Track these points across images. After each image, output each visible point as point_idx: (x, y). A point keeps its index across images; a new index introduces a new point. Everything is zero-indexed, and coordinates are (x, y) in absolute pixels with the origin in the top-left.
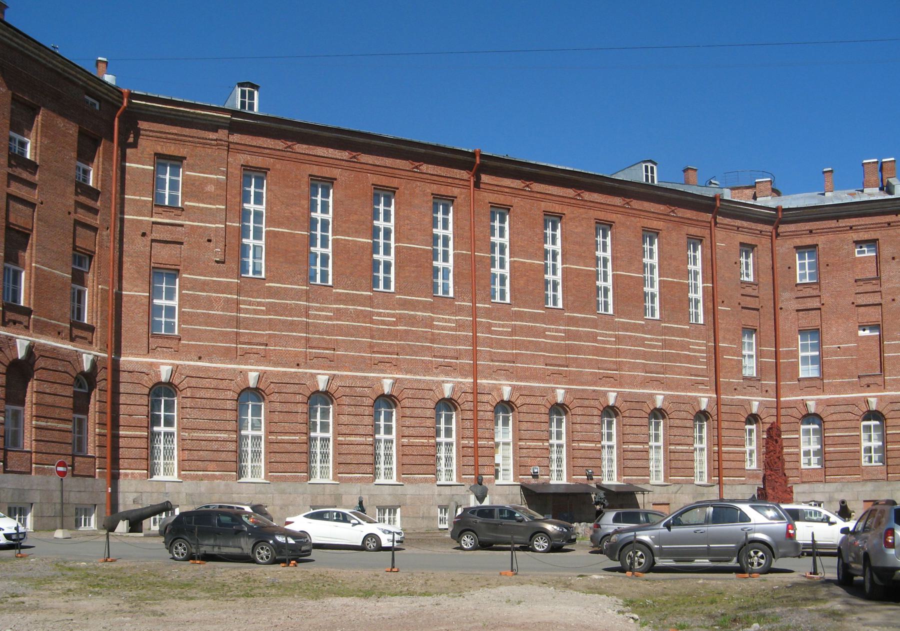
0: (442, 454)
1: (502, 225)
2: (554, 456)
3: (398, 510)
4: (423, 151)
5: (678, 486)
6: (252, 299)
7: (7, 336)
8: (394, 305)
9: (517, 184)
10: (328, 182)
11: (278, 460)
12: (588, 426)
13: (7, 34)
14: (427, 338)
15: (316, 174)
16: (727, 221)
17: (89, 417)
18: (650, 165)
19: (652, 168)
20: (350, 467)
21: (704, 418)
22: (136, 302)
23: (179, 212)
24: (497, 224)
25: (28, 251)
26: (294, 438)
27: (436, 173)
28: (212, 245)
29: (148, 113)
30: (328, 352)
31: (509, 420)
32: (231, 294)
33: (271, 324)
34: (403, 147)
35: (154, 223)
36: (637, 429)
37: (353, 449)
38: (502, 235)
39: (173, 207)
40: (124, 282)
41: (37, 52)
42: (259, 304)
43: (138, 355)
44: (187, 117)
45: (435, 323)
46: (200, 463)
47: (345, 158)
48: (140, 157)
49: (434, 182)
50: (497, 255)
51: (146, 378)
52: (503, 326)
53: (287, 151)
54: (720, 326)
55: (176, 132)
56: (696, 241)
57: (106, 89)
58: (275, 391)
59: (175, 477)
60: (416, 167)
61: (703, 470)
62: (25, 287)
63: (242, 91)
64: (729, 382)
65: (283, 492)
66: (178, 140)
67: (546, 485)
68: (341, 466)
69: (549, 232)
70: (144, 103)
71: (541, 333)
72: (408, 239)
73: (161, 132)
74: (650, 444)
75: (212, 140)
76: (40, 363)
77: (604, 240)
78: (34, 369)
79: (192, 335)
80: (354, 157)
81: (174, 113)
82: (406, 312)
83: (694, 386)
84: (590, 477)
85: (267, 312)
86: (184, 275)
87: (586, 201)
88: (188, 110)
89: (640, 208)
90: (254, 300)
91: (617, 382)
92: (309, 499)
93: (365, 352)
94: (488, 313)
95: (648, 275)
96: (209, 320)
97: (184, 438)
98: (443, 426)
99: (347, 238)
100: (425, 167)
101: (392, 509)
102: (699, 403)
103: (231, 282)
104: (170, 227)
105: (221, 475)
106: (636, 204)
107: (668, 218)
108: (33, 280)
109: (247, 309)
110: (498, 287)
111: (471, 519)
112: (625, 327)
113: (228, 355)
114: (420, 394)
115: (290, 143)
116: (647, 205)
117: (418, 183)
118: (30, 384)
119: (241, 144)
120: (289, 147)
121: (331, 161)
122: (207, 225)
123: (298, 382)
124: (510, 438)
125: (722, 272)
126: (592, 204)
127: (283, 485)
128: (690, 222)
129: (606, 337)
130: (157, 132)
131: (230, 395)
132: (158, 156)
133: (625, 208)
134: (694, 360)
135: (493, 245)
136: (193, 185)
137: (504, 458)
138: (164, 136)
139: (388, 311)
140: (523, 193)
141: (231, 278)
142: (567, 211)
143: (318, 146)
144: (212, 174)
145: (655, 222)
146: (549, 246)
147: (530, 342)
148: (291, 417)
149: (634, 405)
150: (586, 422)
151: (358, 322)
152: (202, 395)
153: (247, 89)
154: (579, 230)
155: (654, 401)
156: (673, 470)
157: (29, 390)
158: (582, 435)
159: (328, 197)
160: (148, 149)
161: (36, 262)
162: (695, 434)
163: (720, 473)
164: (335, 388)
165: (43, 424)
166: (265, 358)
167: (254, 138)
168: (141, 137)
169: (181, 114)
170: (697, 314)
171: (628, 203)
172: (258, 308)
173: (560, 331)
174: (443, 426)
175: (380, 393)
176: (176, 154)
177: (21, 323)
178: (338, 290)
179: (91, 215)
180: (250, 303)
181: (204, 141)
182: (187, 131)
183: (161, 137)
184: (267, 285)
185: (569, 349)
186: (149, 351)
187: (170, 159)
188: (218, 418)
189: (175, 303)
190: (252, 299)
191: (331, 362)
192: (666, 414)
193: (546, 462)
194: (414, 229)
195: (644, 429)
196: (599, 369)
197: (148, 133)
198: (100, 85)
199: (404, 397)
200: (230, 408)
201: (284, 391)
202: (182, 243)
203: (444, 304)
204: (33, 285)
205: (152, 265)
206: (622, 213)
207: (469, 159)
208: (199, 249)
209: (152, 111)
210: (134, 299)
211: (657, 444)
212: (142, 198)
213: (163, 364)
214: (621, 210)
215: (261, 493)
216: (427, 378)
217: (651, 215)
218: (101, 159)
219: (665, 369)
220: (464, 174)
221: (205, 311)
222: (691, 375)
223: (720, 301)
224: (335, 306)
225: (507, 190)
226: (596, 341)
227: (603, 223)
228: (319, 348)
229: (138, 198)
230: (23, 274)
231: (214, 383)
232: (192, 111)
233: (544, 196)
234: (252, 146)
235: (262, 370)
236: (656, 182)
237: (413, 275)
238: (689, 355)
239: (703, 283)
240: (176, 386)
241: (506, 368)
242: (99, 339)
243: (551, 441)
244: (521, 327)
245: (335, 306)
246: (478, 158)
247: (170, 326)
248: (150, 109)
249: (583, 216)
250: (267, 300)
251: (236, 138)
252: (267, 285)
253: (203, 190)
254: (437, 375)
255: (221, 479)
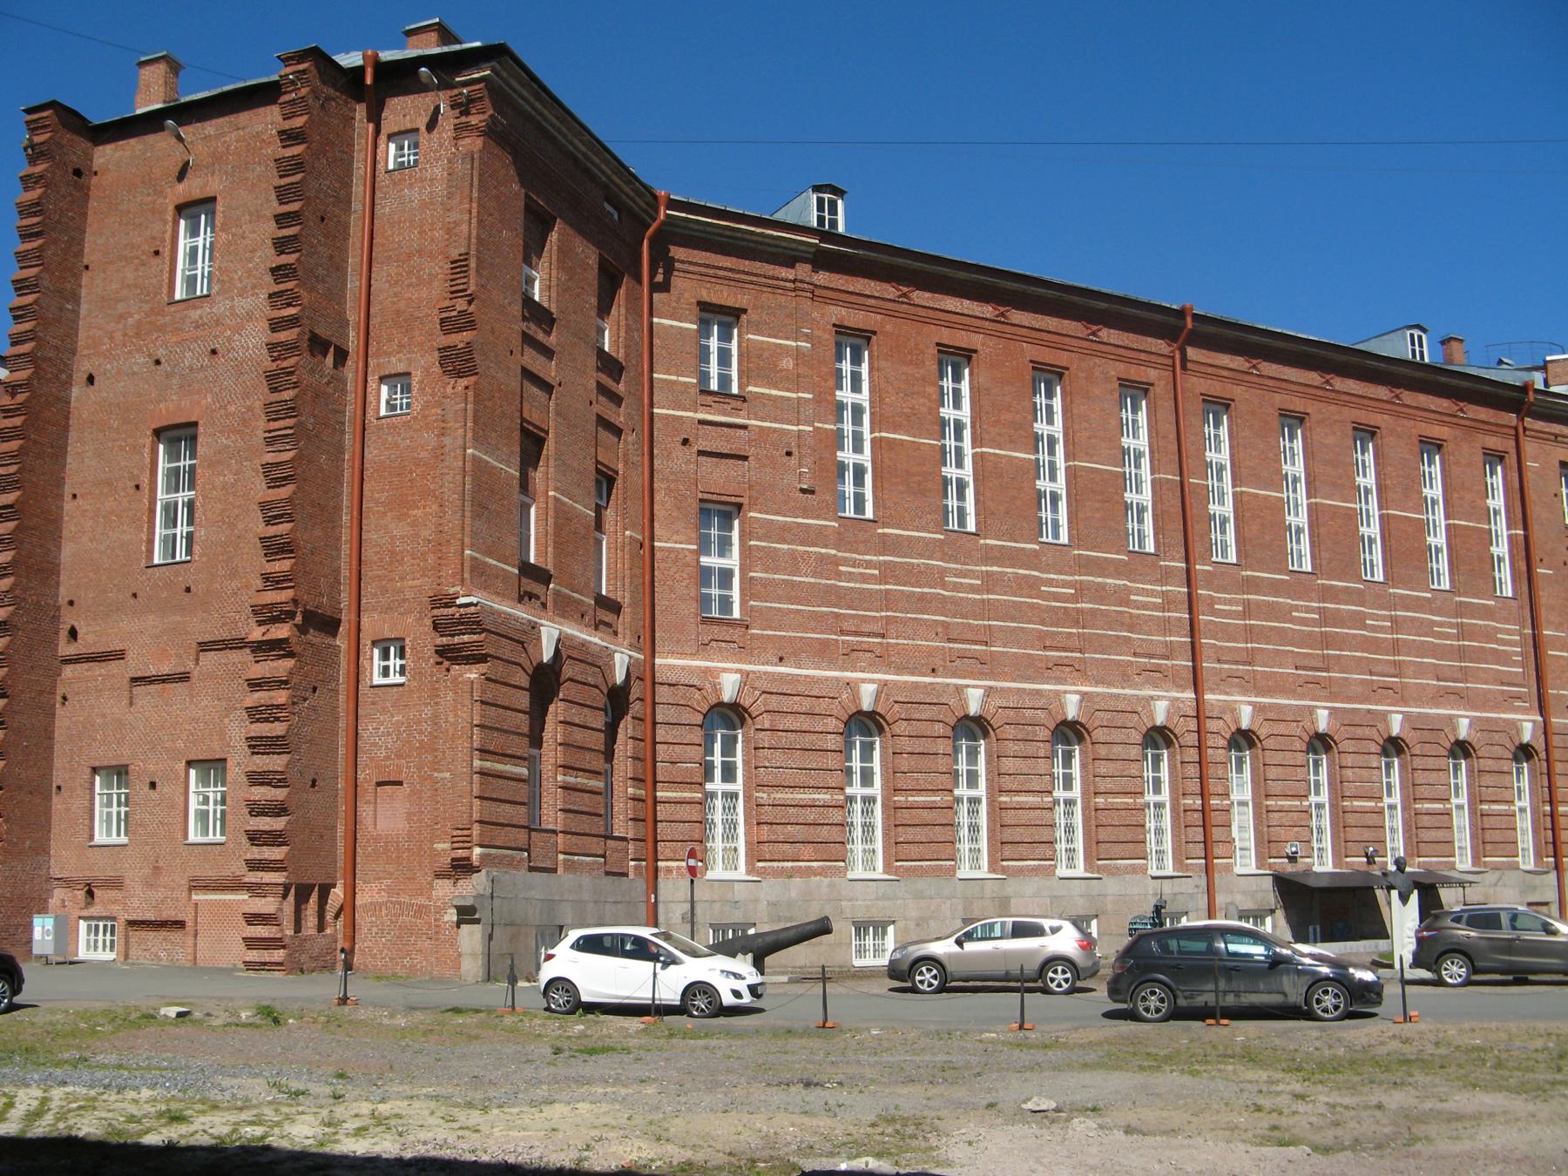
0: (963, 817)
1: (856, 369)
2: (857, 819)
3: (891, 929)
4: (1104, 305)
5: (1497, 874)
6: (858, 557)
7: (529, 621)
8: (1070, 567)
9: (1238, 362)
10: (966, 355)
11: (910, 838)
12: (1364, 772)
13: (525, 94)
14: (1123, 624)
15: (946, 342)
16: (1539, 425)
17: (615, 767)
18: (1416, 333)
19: (1420, 338)
20: (1021, 848)
21: (978, 732)
22: (676, 561)
23: (739, 404)
24: (846, 366)
25: (540, 469)
26: (934, 799)
27: (1121, 343)
28: (793, 461)
29: (687, 232)
30: (977, 647)
31: (872, 749)
32: (826, 547)
33: (888, 600)
34: (1076, 299)
35: (701, 422)
36: (1432, 778)
37: (1025, 817)
38: (856, 388)
39: (724, 394)
40: (656, 525)
41: (558, 124)
42: (869, 565)
43: (682, 655)
44: (748, 241)
45: (1132, 597)
46: (788, 846)
47: (988, 316)
48: (674, 308)
49: (1120, 359)
50: (848, 427)
51: (697, 695)
52: (1230, 602)
53: (903, 303)
54: (1543, 601)
55: (730, 266)
56: (1363, 434)
57: (636, 191)
58: (903, 716)
59: (741, 873)
60: (1094, 334)
61: (1323, 845)
62: (537, 533)
63: (818, 198)
64: (1558, 695)
65: (919, 896)
66: (732, 279)
67: (1308, 872)
68: (1007, 847)
69: (948, 384)
70: (683, 215)
71: (1284, 614)
72: (1087, 454)
73: (708, 266)
74: (957, 792)
75: (786, 280)
76: (568, 670)
77: (957, 386)
78: (562, 680)
79: (770, 619)
80: (1002, 314)
81: (729, 233)
82: (1091, 578)
83: (1508, 701)
84: (1370, 861)
85: (882, 579)
86: (752, 514)
87: (1338, 392)
88: (753, 229)
89: (1414, 404)
90: (861, 557)
91: (1400, 695)
92: (960, 907)
93: (1033, 648)
94: (1210, 579)
95: (1044, 457)
96: (793, 592)
97: (762, 802)
98: (718, 759)
99: (997, 451)
100: (1106, 334)
101: (880, 927)
102: (1519, 731)
103: (826, 526)
104: (725, 429)
105: (822, 867)
106: (1408, 397)
107: (1455, 420)
108: (551, 521)
109: (850, 573)
110: (849, 488)
111: (1455, 932)
112: (1406, 603)
113: (823, 653)
114: (1120, 720)
115: (905, 289)
116: (1424, 400)
117: (1097, 360)
118: (552, 708)
119: (832, 289)
120: (904, 295)
121: (968, 321)
122: (785, 426)
123: (935, 701)
124: (1247, 795)
125: (1537, 511)
126: (1347, 398)
127: (921, 884)
128: (1486, 427)
129: (964, 580)
130: (700, 265)
131: (832, 724)
132: (704, 306)
133: (1394, 403)
134: (1502, 658)
135: (840, 407)
136: (760, 356)
137: (1243, 828)
138: (712, 272)
139: (1062, 577)
140: (1247, 378)
141: (826, 519)
142: (1312, 408)
143: (947, 294)
144: (787, 339)
145: (1437, 428)
146: (947, 412)
147: (1272, 628)
148: (926, 762)
149: (1428, 736)
150: (1360, 764)
151: (1021, 596)
152: (788, 726)
153: (826, 196)
154: (1330, 440)
155: (1455, 729)
156: (1489, 847)
157: (549, 718)
158: (1356, 787)
159: (729, 340)
160: (686, 295)
161: (556, 489)
162: (1145, 774)
163: (1209, 851)
164: (992, 711)
165: (571, 780)
166: (882, 659)
167: (850, 278)
168: (676, 273)
169: (739, 235)
170: (962, 513)
171: (1397, 397)
172: (867, 571)
173: (1311, 610)
174: (718, 759)
175: (1059, 719)
176: (729, 304)
177: (538, 598)
178: (988, 541)
179: (613, 406)
180: (855, 564)
181: (775, 282)
182: (746, 265)
183: (709, 275)
184: (880, 531)
185: (1326, 641)
186: (703, 648)
187: (719, 313)
188: (814, 766)
189: (733, 561)
190: (858, 557)
191: (985, 666)
192: (884, 724)
193: (1304, 833)
194: (1096, 437)
195: (1042, 766)
196: (1371, 673)
197: (685, 267)
198: (628, 183)
199: (1096, 725)
200: (833, 748)
201: (916, 716)
202: (745, 458)
203: (1139, 564)
204: (551, 530)
205: (700, 495)
206: (1391, 413)
207: (1172, 320)
208: (774, 468)
209: (693, 230)
210: (673, 556)
211: (868, 791)
212: (681, 379)
213: (725, 670)
214: (1389, 407)
215: (885, 897)
216: (1128, 691)
217: (1432, 416)
218: (623, 310)
219: (1465, 675)
220: (1160, 346)
221: (786, 577)
222: (1502, 684)
223: (1538, 558)
224: (984, 568)
225: (1225, 373)
226: (1365, 627)
227: (952, 353)
228: (963, 641)
229: (674, 378)
230: (533, 510)
231: (806, 704)
232: (759, 230)
233: (1277, 384)
234: (848, 292)
235: (880, 680)
236: (1427, 360)
237: (1098, 515)
238: (1497, 650)
239: (1509, 528)
240: (746, 710)
241: (1240, 674)
242: (627, 625)
243: (848, 791)
244: (1258, 604)
245: (984, 568)
246: (1189, 320)
247: (726, 603)
248: (691, 225)
249: (1336, 417)
250: (881, 558)
251: (822, 278)
252: (880, 531)
253: (776, 366)
254: (1140, 686)
255: (820, 874)
